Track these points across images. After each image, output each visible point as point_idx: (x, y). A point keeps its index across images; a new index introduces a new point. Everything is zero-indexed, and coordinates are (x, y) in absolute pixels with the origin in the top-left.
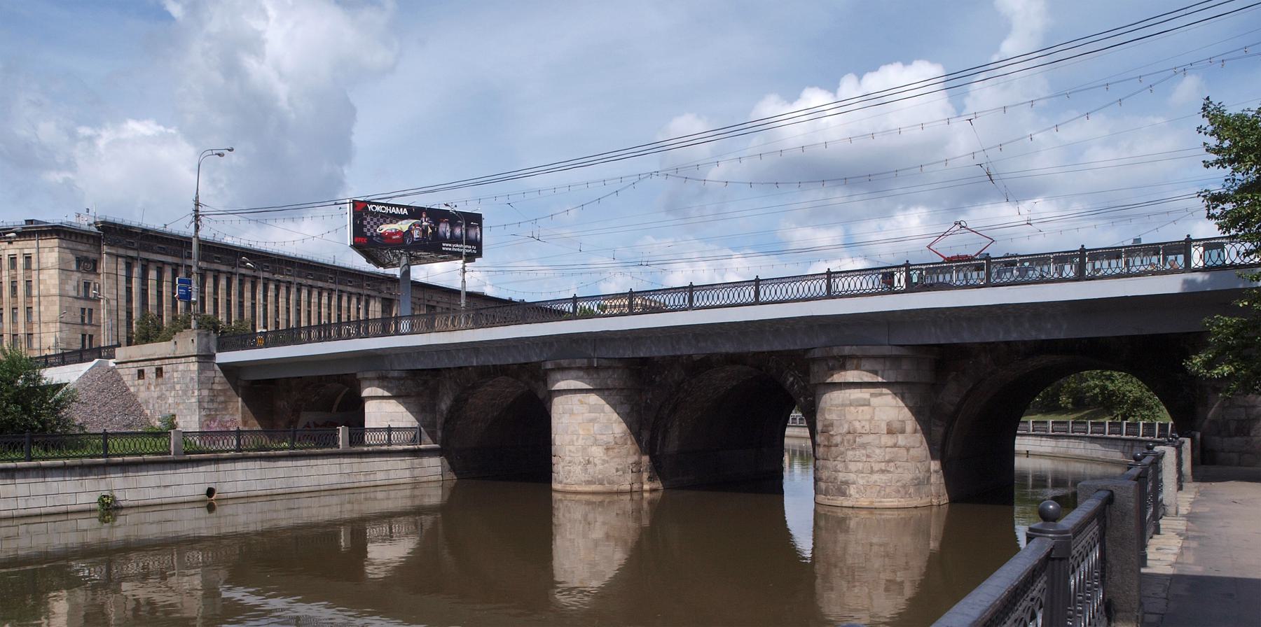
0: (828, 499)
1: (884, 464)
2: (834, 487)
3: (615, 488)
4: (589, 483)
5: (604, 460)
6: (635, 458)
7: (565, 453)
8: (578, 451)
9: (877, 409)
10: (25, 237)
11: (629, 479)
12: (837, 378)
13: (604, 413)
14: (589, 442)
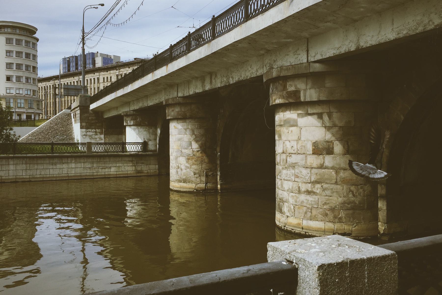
1: (310, 185)
9: (304, 129)
10: (93, 72)
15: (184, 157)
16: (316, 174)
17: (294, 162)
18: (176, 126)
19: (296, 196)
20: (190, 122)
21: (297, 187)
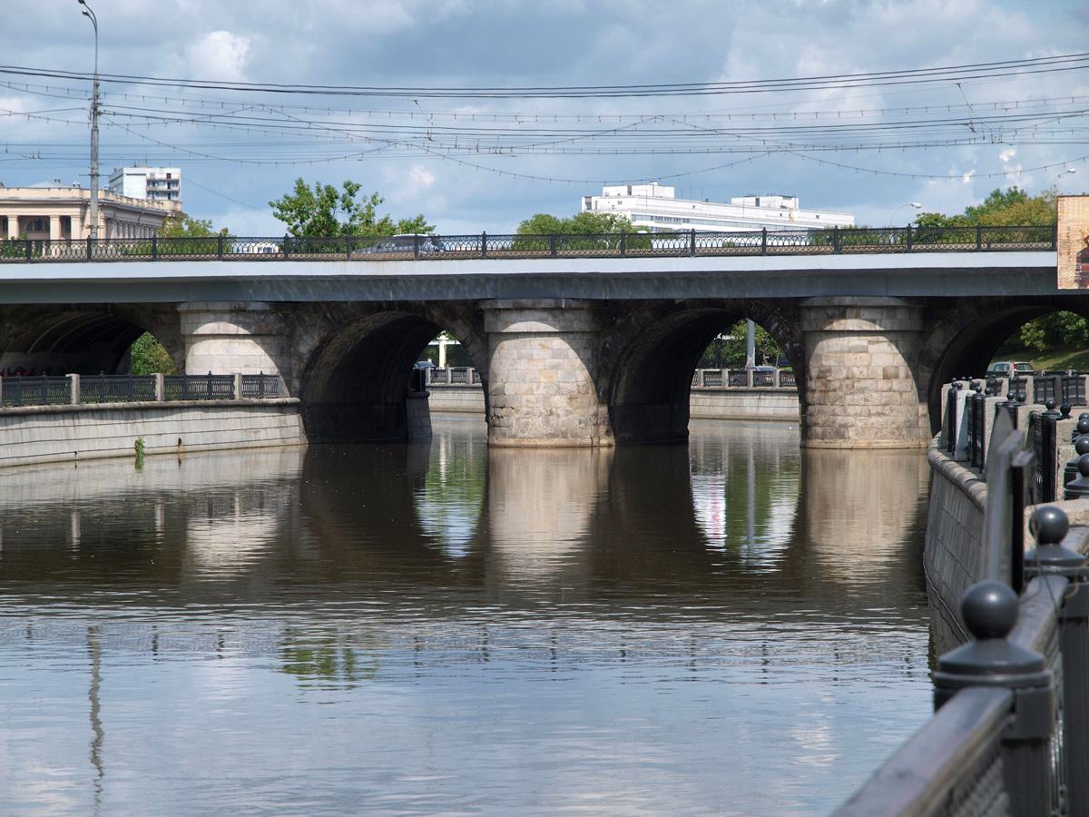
4: (551, 436)
5: (567, 411)
7: (521, 402)
8: (538, 401)
9: (874, 356)
14: (552, 391)
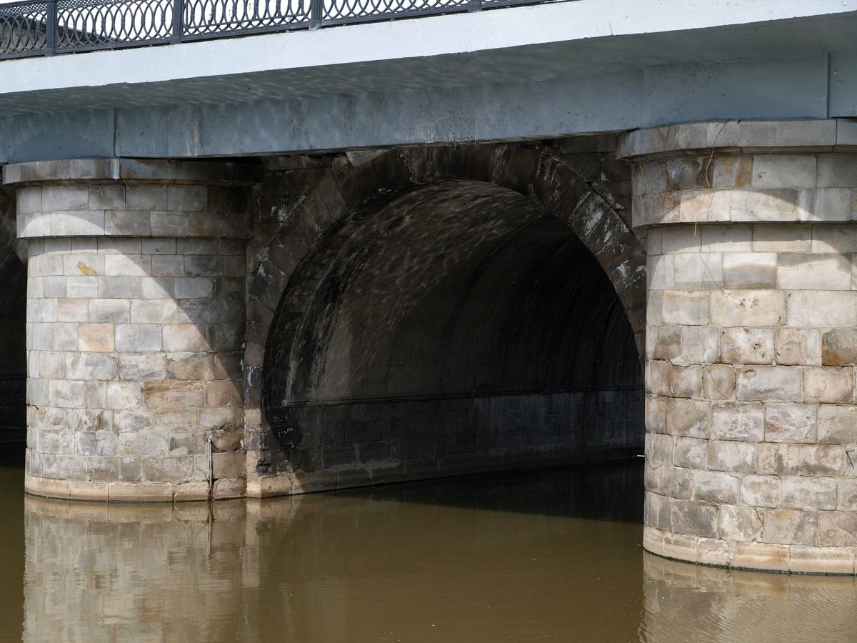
0: (668, 541)
1: (813, 450)
2: (681, 509)
3: (167, 490)
4: (100, 475)
5: (138, 419)
6: (225, 414)
7: (46, 397)
9: (796, 299)
11: (205, 466)
12: (692, 208)
13: (141, 298)
14: (103, 372)
15: (131, 385)
16: (833, 418)
17: (762, 388)
18: (88, 265)
19: (769, 482)
20: (157, 251)
21: (773, 459)
